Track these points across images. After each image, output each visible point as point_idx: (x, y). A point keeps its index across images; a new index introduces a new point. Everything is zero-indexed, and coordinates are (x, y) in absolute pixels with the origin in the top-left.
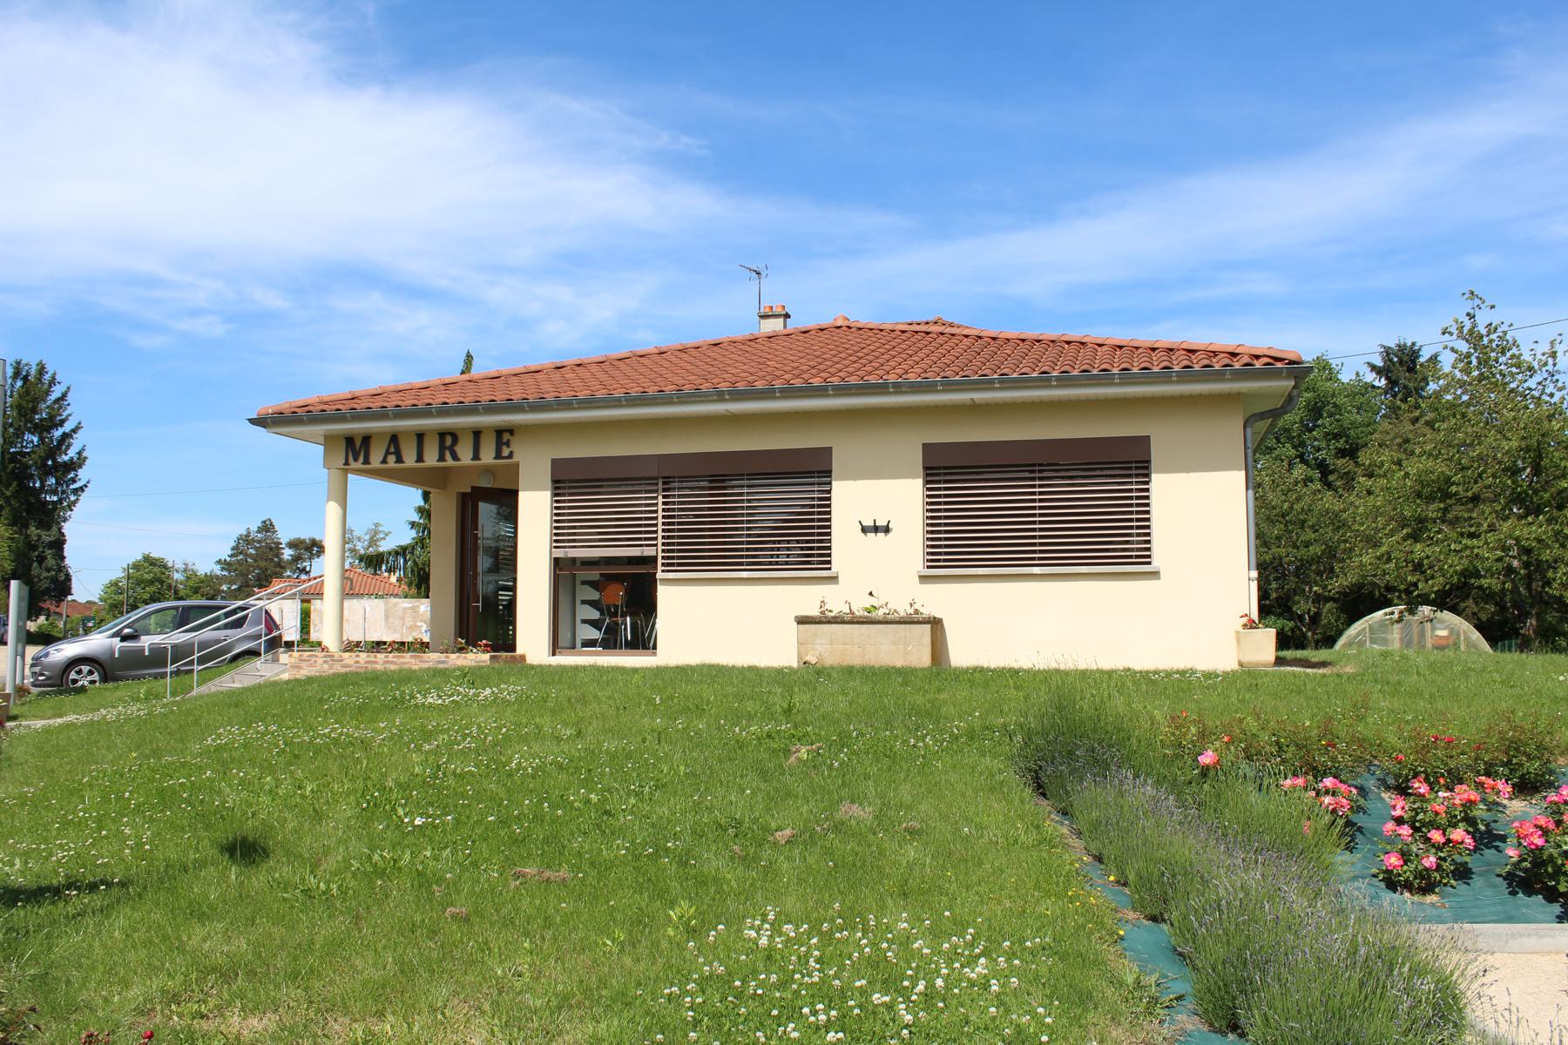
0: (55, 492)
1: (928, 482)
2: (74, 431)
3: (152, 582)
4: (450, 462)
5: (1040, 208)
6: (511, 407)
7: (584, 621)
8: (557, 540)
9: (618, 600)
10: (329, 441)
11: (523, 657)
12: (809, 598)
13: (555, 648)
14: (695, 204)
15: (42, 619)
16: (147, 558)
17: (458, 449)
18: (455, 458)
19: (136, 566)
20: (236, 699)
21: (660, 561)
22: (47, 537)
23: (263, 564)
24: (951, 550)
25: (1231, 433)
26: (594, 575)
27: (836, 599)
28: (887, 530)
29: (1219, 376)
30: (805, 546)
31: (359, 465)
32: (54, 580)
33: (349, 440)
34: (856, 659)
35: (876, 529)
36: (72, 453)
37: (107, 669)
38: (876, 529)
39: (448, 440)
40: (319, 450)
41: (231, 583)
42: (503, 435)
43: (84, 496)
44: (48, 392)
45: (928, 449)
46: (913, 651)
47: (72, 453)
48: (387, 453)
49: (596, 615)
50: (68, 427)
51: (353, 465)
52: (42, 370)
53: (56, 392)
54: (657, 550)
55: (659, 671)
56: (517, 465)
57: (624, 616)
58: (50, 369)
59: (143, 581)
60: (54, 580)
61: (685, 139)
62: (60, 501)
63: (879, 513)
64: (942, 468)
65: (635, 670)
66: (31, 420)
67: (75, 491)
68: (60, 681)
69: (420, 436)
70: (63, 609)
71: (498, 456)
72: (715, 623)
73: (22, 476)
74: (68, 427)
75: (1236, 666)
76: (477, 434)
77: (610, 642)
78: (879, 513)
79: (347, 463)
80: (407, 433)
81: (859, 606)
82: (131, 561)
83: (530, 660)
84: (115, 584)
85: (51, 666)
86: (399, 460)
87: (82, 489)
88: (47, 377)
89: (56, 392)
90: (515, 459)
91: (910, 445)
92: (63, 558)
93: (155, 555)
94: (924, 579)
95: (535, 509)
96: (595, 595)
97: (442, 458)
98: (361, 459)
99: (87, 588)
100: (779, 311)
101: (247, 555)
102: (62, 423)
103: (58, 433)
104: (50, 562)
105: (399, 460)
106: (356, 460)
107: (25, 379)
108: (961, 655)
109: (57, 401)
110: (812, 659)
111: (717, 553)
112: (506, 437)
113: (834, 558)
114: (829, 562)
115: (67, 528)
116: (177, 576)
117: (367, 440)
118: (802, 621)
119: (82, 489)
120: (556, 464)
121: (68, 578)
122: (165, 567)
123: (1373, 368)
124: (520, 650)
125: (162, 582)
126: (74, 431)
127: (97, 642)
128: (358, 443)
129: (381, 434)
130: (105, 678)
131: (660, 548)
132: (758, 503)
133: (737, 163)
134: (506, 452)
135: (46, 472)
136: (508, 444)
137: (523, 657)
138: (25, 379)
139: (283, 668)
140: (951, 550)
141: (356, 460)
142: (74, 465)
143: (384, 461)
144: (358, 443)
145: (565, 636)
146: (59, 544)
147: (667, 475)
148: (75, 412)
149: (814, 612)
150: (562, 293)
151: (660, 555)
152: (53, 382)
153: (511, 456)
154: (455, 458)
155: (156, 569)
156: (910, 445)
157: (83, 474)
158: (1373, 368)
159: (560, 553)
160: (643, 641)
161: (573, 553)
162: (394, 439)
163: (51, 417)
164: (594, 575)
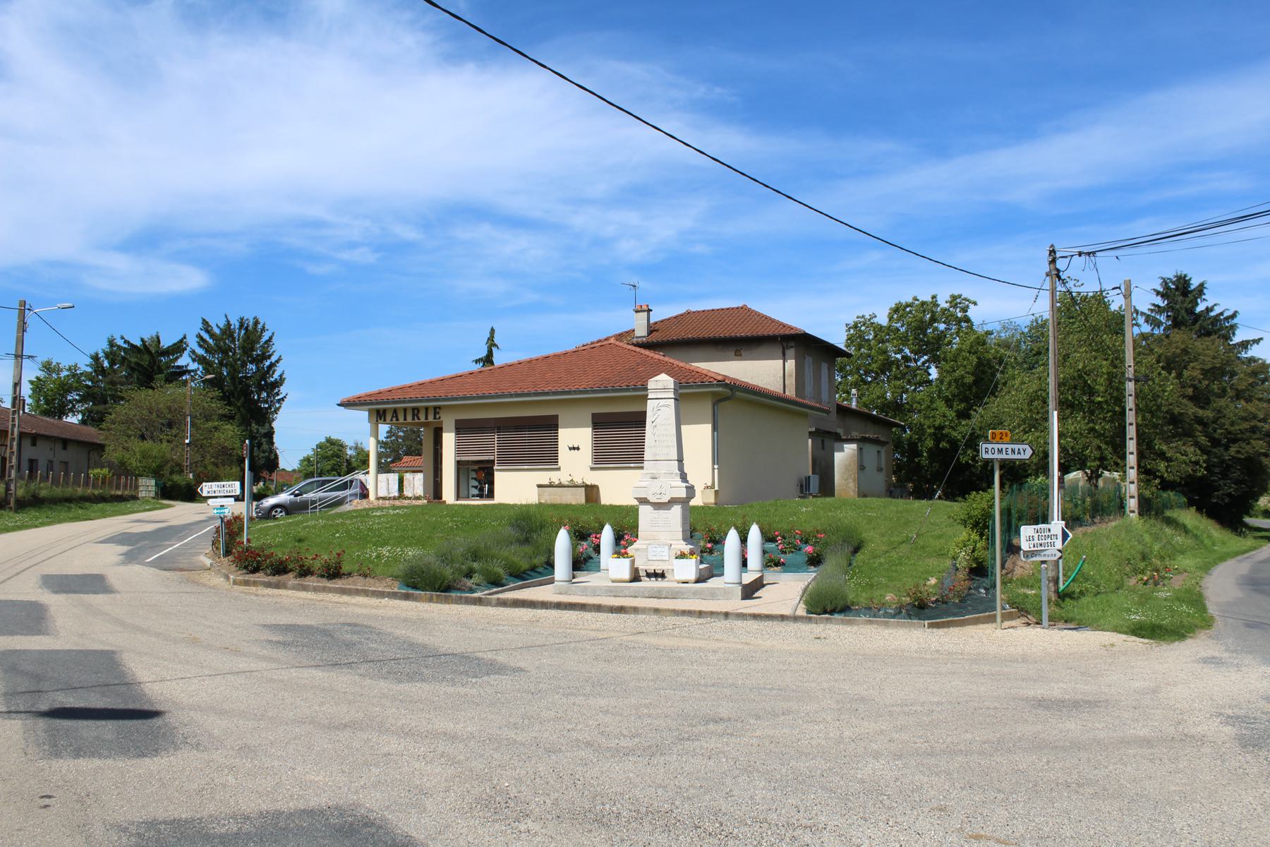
0: (266, 402)
2: (277, 362)
3: (333, 456)
5: (1023, 129)
9: (479, 476)
10: (370, 411)
12: (544, 477)
14: (732, 142)
15: (261, 484)
16: (329, 440)
22: (262, 431)
23: (409, 443)
25: (707, 408)
26: (476, 467)
27: (555, 477)
30: (548, 457)
32: (268, 458)
33: (378, 411)
34: (557, 500)
36: (276, 376)
37: (288, 509)
39: (416, 411)
40: (366, 413)
41: (387, 457)
42: (437, 410)
43: (284, 404)
44: (260, 337)
46: (579, 498)
47: (276, 376)
50: (273, 359)
52: (256, 323)
53: (266, 337)
54: (494, 457)
58: (261, 321)
60: (268, 458)
61: (718, 90)
62: (270, 407)
63: (575, 441)
64: (599, 423)
66: (251, 356)
67: (279, 401)
68: (268, 514)
69: (405, 410)
70: (274, 476)
73: (246, 393)
74: (273, 359)
76: (427, 409)
77: (481, 496)
78: (575, 441)
81: (565, 481)
84: (307, 459)
85: (263, 509)
87: (283, 399)
88: (260, 326)
89: (266, 337)
92: (273, 443)
94: (592, 469)
95: (449, 439)
99: (289, 459)
101: (398, 437)
102: (269, 357)
103: (267, 363)
104: (265, 446)
107: (247, 329)
109: (267, 342)
111: (515, 460)
115: (274, 425)
116: (349, 452)
117: (385, 411)
118: (539, 486)
119: (283, 399)
121: (276, 457)
122: (342, 446)
123: (1158, 293)
125: (338, 456)
126: (277, 362)
127: (284, 497)
130: (287, 514)
132: (531, 436)
133: (763, 107)
135: (261, 389)
138: (247, 329)
140: (603, 458)
142: (280, 381)
146: (270, 435)
147: (500, 426)
148: (278, 349)
149: (547, 482)
150: (632, 217)
152: (263, 329)
155: (336, 448)
157: (283, 390)
158: (1158, 293)
160: (491, 494)
162: (395, 411)
163: (263, 354)
164: (476, 467)
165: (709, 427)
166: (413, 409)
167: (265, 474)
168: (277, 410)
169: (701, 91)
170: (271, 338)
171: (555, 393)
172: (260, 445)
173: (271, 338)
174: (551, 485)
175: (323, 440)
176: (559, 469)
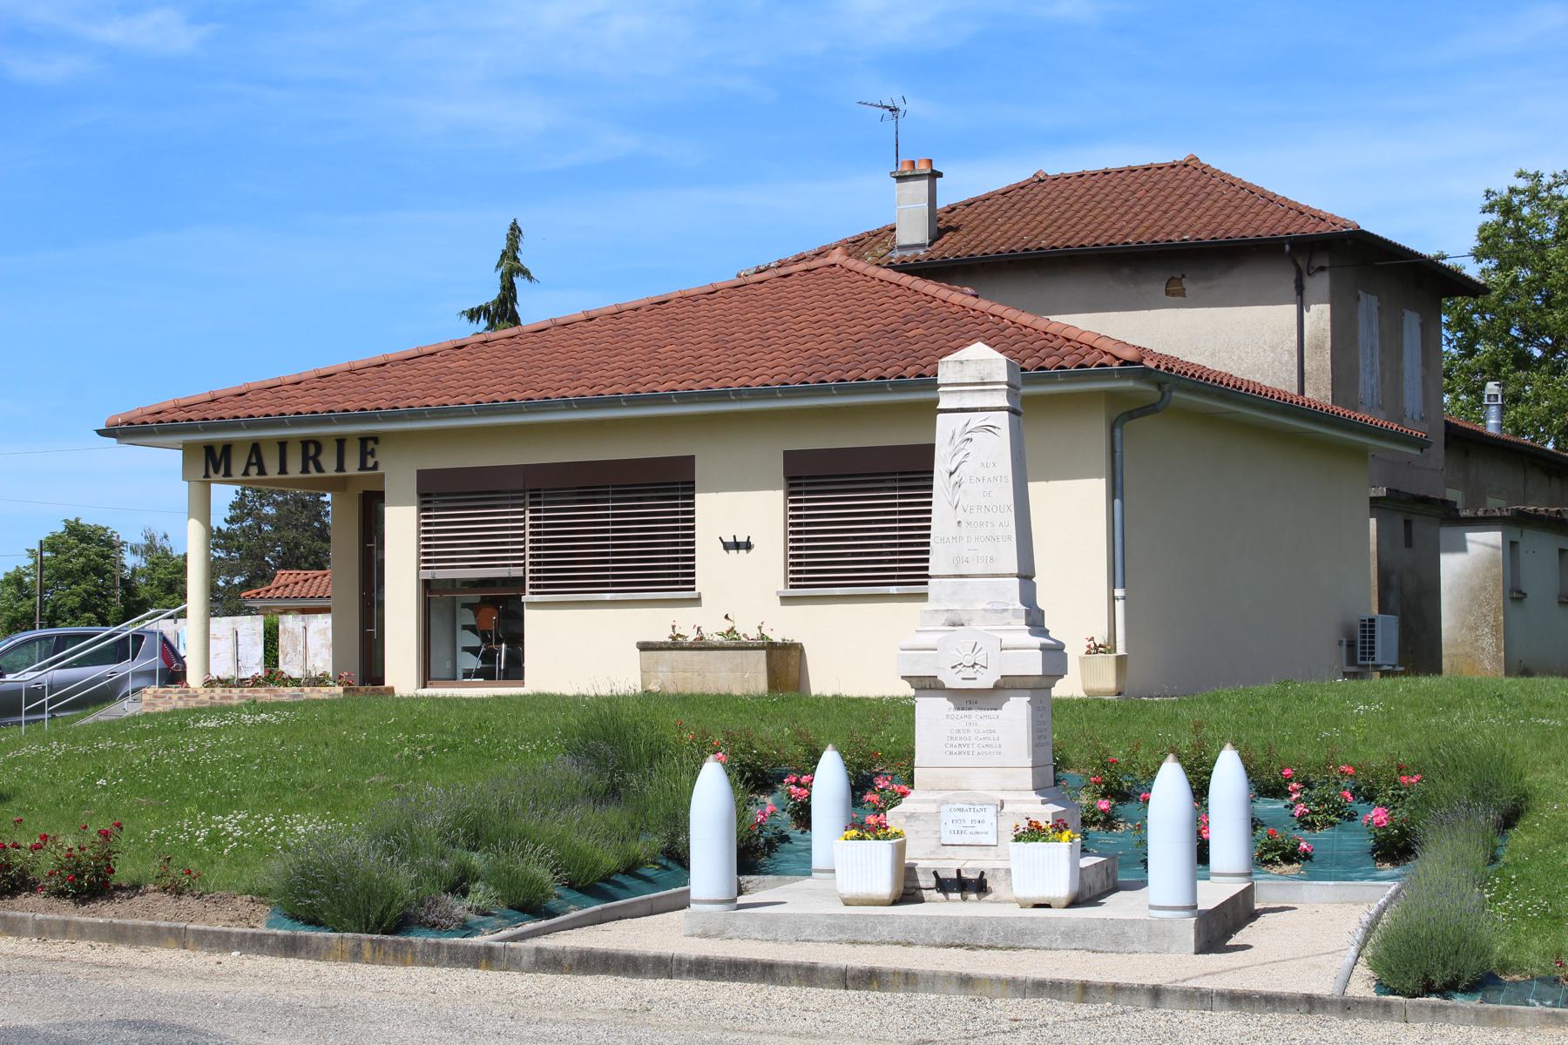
1: (792, 493)
3: (84, 572)
4: (314, 473)
6: (370, 418)
7: (466, 649)
8: (427, 556)
9: (482, 621)
10: (187, 449)
11: (391, 690)
12: (656, 622)
13: (426, 678)
17: (321, 458)
18: (319, 469)
19: (52, 544)
20: (110, 728)
21: (528, 582)
24: (815, 569)
26: (475, 597)
27: (686, 622)
28: (748, 546)
29: (1051, 379)
30: (667, 569)
31: (220, 476)
33: (209, 449)
35: (737, 546)
38: (737, 546)
40: (178, 455)
41: (233, 572)
42: (367, 444)
45: (788, 456)
46: (751, 677)
48: (249, 464)
49: (475, 641)
51: (214, 477)
55: (523, 699)
56: (383, 475)
57: (499, 642)
59: (69, 573)
63: (741, 522)
64: (805, 477)
65: (468, 700)
71: (363, 467)
72: (581, 650)
75: (1082, 695)
76: (341, 442)
77: (487, 674)
78: (741, 522)
79: (207, 476)
80: (269, 440)
81: (713, 629)
82: (44, 535)
83: (398, 692)
86: (262, 472)
90: (380, 471)
91: (770, 454)
93: (89, 519)
94: (785, 600)
95: (401, 525)
96: (472, 621)
97: (305, 470)
98: (222, 471)
100: (922, 168)
101: (261, 519)
105: (262, 472)
106: (216, 471)
108: (824, 680)
110: (654, 687)
111: (581, 574)
112: (371, 445)
113: (697, 578)
114: (693, 582)
116: (130, 560)
117: (227, 448)
118: (645, 647)
120: (423, 476)
124: (388, 683)
125: (99, 572)
128: (218, 452)
129: (242, 442)
131: (528, 567)
132: (626, 522)
134: (370, 463)
136: (372, 453)
137: (391, 690)
139: (156, 699)
140: (815, 569)
141: (216, 471)
143: (246, 473)
144: (218, 452)
145: (440, 664)
149: (664, 636)
151: (528, 575)
153: (375, 467)
154: (319, 469)
155: (93, 549)
156: (770, 454)
159: (427, 574)
160: (515, 670)
161: (441, 574)
162: (256, 448)
164: (475, 597)
166: (305, 443)
174: (675, 645)
175: (60, 528)
176: (697, 601)
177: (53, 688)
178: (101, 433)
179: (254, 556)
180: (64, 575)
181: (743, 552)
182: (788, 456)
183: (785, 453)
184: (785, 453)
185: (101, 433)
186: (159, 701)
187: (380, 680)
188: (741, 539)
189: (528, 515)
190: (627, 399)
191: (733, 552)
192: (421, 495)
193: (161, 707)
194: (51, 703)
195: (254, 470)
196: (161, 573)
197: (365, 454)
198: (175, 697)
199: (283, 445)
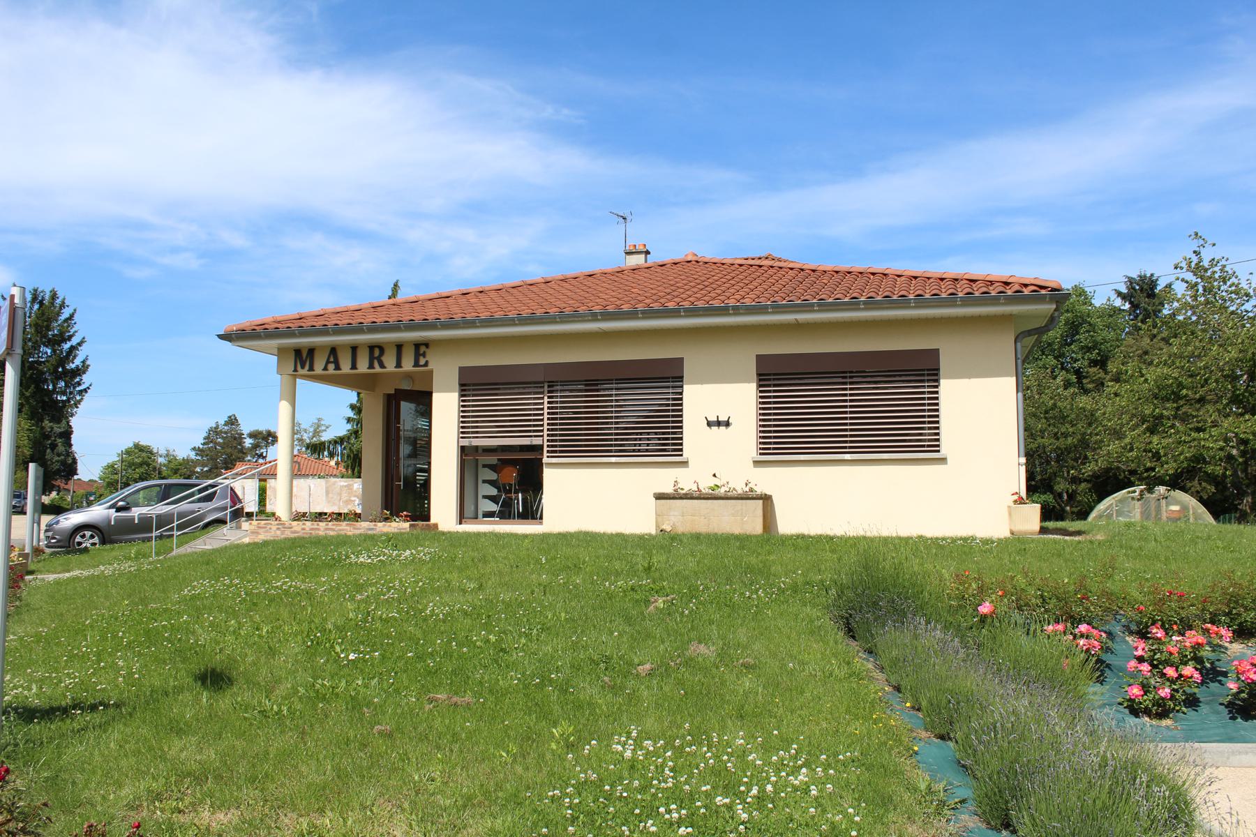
0: (64, 393)
2: (80, 344)
3: (141, 465)
4: (378, 369)
7: (485, 497)
8: (464, 431)
9: (512, 480)
10: (281, 352)
11: (436, 526)
12: (664, 478)
15: (54, 494)
16: (137, 446)
17: (384, 359)
18: (382, 366)
19: (128, 452)
21: (545, 449)
22: (58, 429)
23: (229, 450)
24: (779, 440)
25: (1004, 347)
26: (493, 460)
27: (686, 479)
28: (727, 424)
29: (995, 301)
30: (662, 437)
31: (305, 372)
32: (64, 463)
33: (298, 352)
34: (702, 527)
35: (718, 423)
36: (78, 362)
37: (104, 534)
38: (718, 423)
39: (375, 351)
41: (204, 466)
42: (420, 348)
43: (87, 397)
44: (59, 314)
45: (760, 358)
46: (748, 521)
47: (78, 362)
48: (328, 362)
49: (493, 492)
50: (74, 341)
51: (301, 372)
52: (54, 296)
53: (66, 313)
54: (543, 440)
55: (545, 537)
56: (431, 372)
58: (61, 295)
59: (133, 464)
60: (64, 463)
61: (566, 111)
62: (69, 400)
63: (721, 410)
64: (771, 375)
65: (525, 536)
66: (46, 336)
67: (80, 392)
68: (68, 544)
70: (71, 486)
71: (416, 364)
72: (589, 498)
74: (74, 341)
76: (399, 347)
77: (506, 513)
78: (721, 410)
79: (295, 370)
80: (343, 346)
81: (706, 484)
83: (442, 528)
85: (61, 532)
86: (338, 368)
87: (85, 390)
88: (58, 301)
89: (66, 313)
90: (430, 367)
91: (746, 356)
92: (71, 445)
94: (757, 463)
95: (446, 408)
97: (371, 366)
99: (89, 469)
102: (70, 338)
103: (66, 346)
104: (61, 448)
105: (338, 368)
106: (303, 367)
107: (41, 303)
108: (787, 525)
109: (66, 320)
111: (591, 442)
112: (423, 349)
113: (685, 447)
115: (74, 422)
116: (161, 460)
117: (311, 351)
118: (659, 497)
119: (85, 390)
121: (75, 461)
122: (151, 453)
124: (433, 520)
125: (148, 465)
126: (80, 344)
127: (98, 513)
128: (304, 355)
129: (322, 347)
131: (546, 438)
132: (624, 403)
133: (608, 130)
134: (422, 361)
135: (58, 377)
136: (424, 355)
137: (436, 526)
138: (41, 303)
140: (779, 440)
141: (303, 367)
142: (83, 369)
143: (325, 369)
144: (304, 355)
146: (67, 434)
147: (551, 379)
148: (80, 329)
149: (669, 490)
150: (468, 234)
151: (546, 444)
152: (63, 305)
153: (426, 364)
154: (382, 366)
155: (144, 455)
156: (746, 356)
157: (86, 379)
159: (465, 442)
160: (532, 513)
161: (476, 442)
162: (333, 351)
163: (62, 334)
164: (493, 460)
165: (1012, 381)
166: (372, 348)
167: (59, 482)
168: (76, 405)
169: (549, 112)
170: (71, 317)
171: (693, 312)
172: (54, 446)
173: (71, 317)
174: (676, 496)
175: (131, 445)
176: (685, 464)
177: (181, 515)
178: (221, 337)
179: (213, 459)
180: (131, 465)
181: (723, 428)
182: (760, 358)
183: (757, 356)
184: (757, 356)
185: (221, 337)
186: (261, 531)
187: (427, 518)
188: (723, 418)
189: (546, 400)
190: (643, 312)
191: (715, 428)
192: (461, 385)
193: (261, 537)
194: (180, 527)
195: (331, 366)
196: (172, 465)
197: (418, 355)
198: (274, 528)
199: (354, 349)
